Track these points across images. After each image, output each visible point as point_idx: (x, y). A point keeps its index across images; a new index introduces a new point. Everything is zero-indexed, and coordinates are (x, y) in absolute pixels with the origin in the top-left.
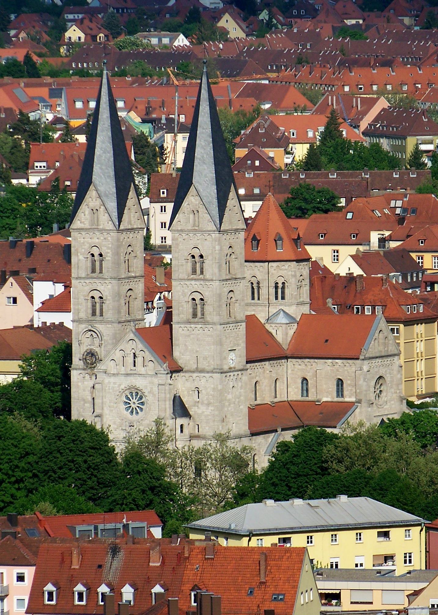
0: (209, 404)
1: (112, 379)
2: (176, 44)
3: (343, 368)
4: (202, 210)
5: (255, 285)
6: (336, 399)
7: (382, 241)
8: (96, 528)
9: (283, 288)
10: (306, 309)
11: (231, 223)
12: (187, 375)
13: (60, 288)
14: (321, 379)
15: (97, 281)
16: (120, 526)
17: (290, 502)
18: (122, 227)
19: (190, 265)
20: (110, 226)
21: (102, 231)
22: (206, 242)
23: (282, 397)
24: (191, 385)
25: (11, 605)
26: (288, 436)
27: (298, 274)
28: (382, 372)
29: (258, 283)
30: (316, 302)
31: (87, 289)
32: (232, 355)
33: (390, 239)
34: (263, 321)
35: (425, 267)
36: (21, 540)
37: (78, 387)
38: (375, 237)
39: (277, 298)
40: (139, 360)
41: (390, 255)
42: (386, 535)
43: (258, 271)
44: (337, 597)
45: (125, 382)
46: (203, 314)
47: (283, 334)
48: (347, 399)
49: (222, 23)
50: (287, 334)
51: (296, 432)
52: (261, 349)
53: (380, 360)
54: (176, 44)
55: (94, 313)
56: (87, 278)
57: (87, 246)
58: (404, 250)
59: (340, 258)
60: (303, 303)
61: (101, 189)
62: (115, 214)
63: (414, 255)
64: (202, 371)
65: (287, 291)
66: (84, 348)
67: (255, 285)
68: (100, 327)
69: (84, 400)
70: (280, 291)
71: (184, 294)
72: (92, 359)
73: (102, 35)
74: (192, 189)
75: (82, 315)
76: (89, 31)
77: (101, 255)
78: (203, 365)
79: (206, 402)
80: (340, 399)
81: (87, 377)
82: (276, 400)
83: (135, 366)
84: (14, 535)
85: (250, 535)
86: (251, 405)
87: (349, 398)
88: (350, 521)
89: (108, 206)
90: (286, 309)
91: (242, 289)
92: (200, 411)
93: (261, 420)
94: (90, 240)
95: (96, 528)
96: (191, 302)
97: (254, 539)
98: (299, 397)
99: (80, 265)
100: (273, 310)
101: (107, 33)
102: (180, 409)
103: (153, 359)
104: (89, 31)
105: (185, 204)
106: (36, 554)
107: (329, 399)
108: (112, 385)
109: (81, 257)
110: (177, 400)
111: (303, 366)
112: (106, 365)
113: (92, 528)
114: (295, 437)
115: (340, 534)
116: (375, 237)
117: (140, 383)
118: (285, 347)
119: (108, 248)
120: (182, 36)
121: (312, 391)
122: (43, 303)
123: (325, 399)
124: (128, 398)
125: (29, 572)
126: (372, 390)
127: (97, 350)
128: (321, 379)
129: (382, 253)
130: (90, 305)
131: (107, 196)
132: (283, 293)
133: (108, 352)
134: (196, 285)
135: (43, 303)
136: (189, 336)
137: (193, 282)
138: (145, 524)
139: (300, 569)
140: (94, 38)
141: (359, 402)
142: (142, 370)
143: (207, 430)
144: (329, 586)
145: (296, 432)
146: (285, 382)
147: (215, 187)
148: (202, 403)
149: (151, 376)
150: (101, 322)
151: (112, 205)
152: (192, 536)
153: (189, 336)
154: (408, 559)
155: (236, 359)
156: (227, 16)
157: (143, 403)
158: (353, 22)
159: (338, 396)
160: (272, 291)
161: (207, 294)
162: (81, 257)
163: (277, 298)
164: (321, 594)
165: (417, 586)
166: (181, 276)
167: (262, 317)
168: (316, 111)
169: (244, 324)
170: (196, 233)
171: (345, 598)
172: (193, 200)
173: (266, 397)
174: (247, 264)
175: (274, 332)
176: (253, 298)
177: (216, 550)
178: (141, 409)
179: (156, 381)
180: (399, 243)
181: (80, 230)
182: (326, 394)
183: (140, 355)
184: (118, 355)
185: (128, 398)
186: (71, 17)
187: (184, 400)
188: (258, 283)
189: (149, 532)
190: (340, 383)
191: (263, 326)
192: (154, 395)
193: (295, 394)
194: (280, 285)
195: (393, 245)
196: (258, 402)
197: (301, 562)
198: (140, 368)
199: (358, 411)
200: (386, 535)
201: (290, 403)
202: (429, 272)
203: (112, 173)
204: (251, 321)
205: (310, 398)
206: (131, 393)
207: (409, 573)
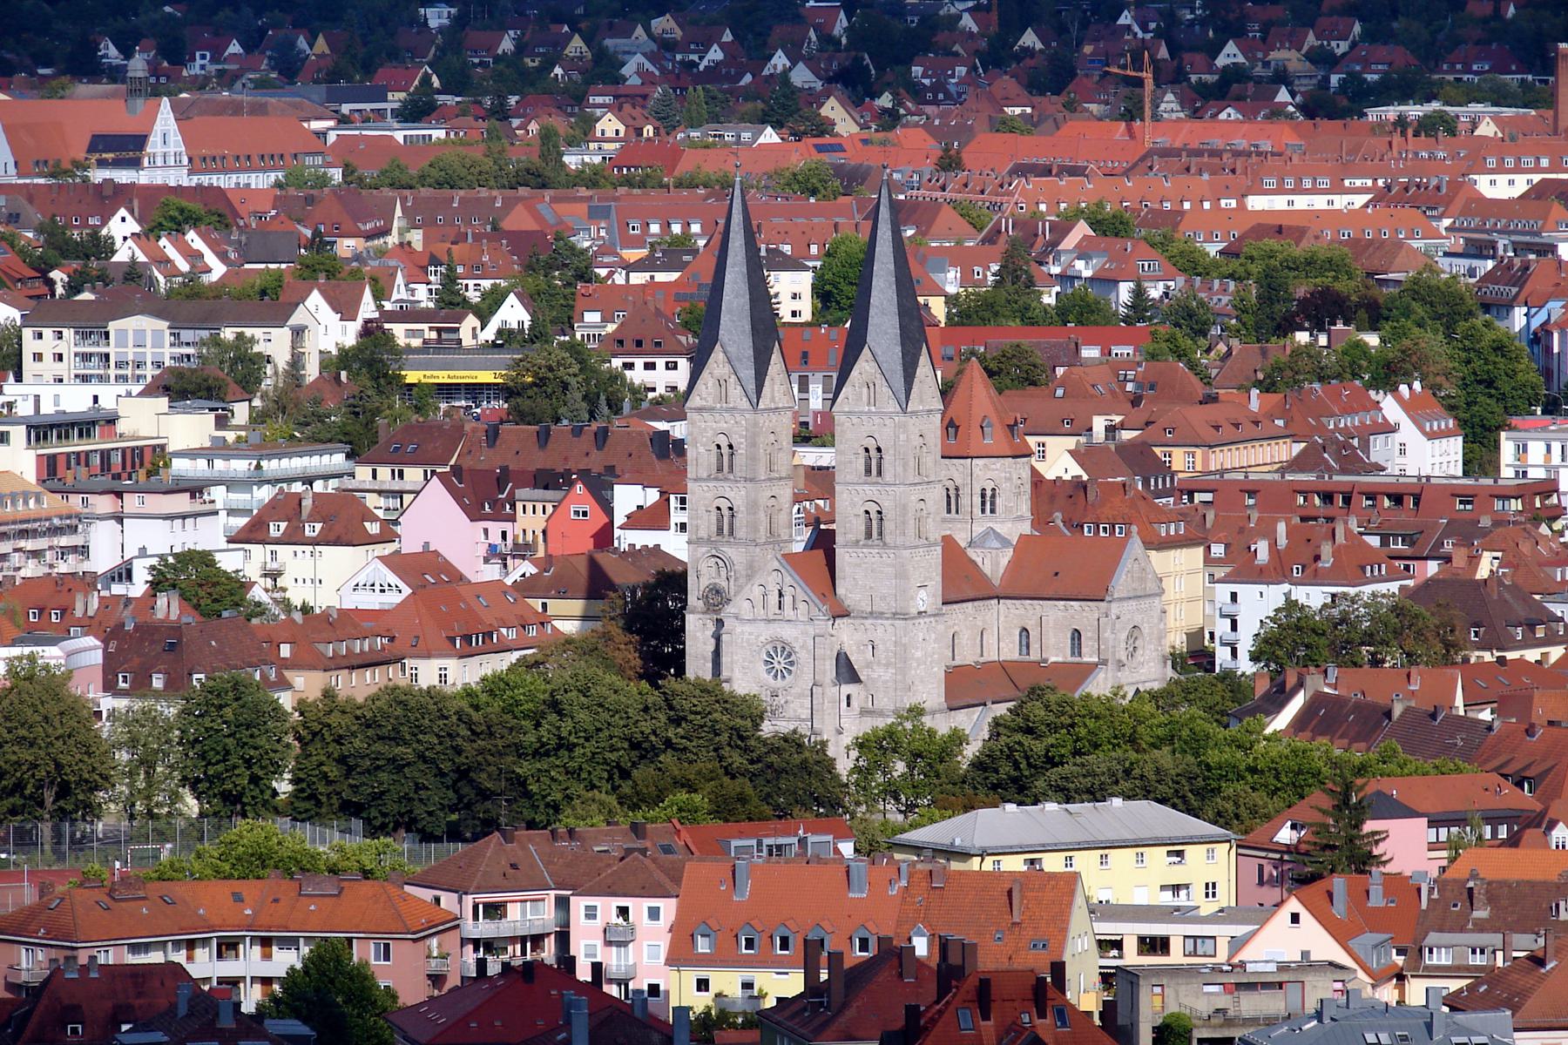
0: (887, 665)
1: (748, 628)
2: (762, 140)
3: (1081, 614)
4: (880, 381)
5: (952, 493)
6: (1070, 659)
7: (1111, 430)
8: (760, 844)
9: (993, 496)
10: (1026, 528)
11: (921, 401)
12: (857, 622)
13: (653, 495)
14: (1052, 630)
16: (795, 840)
17: (1040, 806)
18: (761, 406)
19: (862, 461)
20: (745, 404)
23: (991, 655)
24: (861, 636)
25: (639, 952)
26: (1001, 710)
27: (1015, 477)
28: (1137, 620)
29: (957, 489)
30: (1040, 519)
31: (710, 495)
32: (922, 594)
33: (1122, 426)
34: (963, 544)
35: (1174, 468)
36: (654, 860)
37: (696, 638)
38: (1099, 424)
39: (983, 511)
40: (787, 600)
41: (1123, 448)
42: (1180, 854)
43: (957, 469)
44: (1118, 945)
45: (765, 632)
46: (880, 534)
47: (994, 563)
48: (1086, 659)
49: (825, 111)
50: (998, 564)
51: (1011, 705)
52: (963, 583)
53: (1133, 603)
54: (762, 140)
55: (720, 531)
56: (709, 478)
57: (710, 434)
58: (1144, 443)
59: (1047, 454)
60: (1020, 518)
61: (731, 349)
62: (751, 387)
63: (1157, 450)
64: (881, 615)
65: (998, 501)
66: (704, 582)
67: (952, 493)
68: (729, 552)
70: (988, 501)
71: (853, 505)
72: (717, 599)
73: (650, 128)
74: (866, 350)
75: (703, 533)
76: (631, 122)
77: (731, 447)
78: (880, 606)
80: (1077, 659)
82: (982, 660)
84: (643, 851)
85: (983, 855)
87: (1089, 657)
88: (1128, 835)
89: (741, 375)
90: (998, 528)
91: (936, 495)
92: (875, 675)
93: (964, 685)
95: (760, 844)
96: (863, 515)
97: (989, 860)
98: (1015, 656)
100: (978, 529)
101: (658, 124)
102: (847, 671)
104: (631, 122)
105: (855, 373)
106: (677, 880)
107: (1060, 659)
108: (746, 636)
109: (702, 450)
110: (842, 661)
111: (1022, 611)
112: (739, 606)
113: (754, 842)
114: (1009, 710)
115: (1113, 854)
116: (1099, 424)
117: (788, 633)
118: (997, 582)
120: (769, 129)
121: (1035, 646)
122: (628, 517)
123: (1053, 659)
124: (770, 655)
125: (668, 907)
126: (1123, 645)
127: (724, 584)
128: (1052, 630)
129: (1113, 447)
130: (714, 519)
131: (740, 360)
132: (993, 504)
133: (740, 589)
134: (870, 491)
135: (628, 517)
136: (859, 565)
137: (866, 487)
138: (830, 838)
139: (1070, 904)
140: (639, 132)
141: (1105, 662)
143: (885, 702)
144: (1108, 929)
145: (1011, 705)
146: (994, 632)
147: (898, 349)
148: (879, 663)
151: (748, 373)
152: (897, 856)
153: (859, 565)
154: (1211, 889)
155: (926, 599)
156: (832, 101)
157: (792, 663)
158: (1018, 110)
159: (1073, 654)
160: (977, 500)
161: (887, 505)
162: (702, 450)
163: (983, 511)
164: (1100, 942)
165: (1240, 930)
166: (849, 478)
167: (962, 539)
168: (983, 241)
169: (939, 549)
170: (887, 415)
171: (1176, 946)
173: (967, 655)
174: (947, 461)
175: (979, 561)
176: (949, 511)
177: (948, 876)
178: (790, 672)
180: (1136, 433)
181: (700, 410)
182: (1057, 652)
183: (788, 592)
184: (757, 592)
185: (770, 655)
186: (599, 100)
187: (852, 659)
188: (957, 489)
189: (837, 851)
190: (1076, 635)
191: (963, 552)
193: (1010, 652)
194: (989, 493)
195: (1126, 435)
196: (957, 662)
197: (1072, 893)
198: (788, 611)
199: (1102, 675)
200: (1180, 854)
201: (1003, 666)
202: (1181, 475)
203: (748, 327)
204: (948, 543)
205: (1032, 658)
207: (1221, 911)
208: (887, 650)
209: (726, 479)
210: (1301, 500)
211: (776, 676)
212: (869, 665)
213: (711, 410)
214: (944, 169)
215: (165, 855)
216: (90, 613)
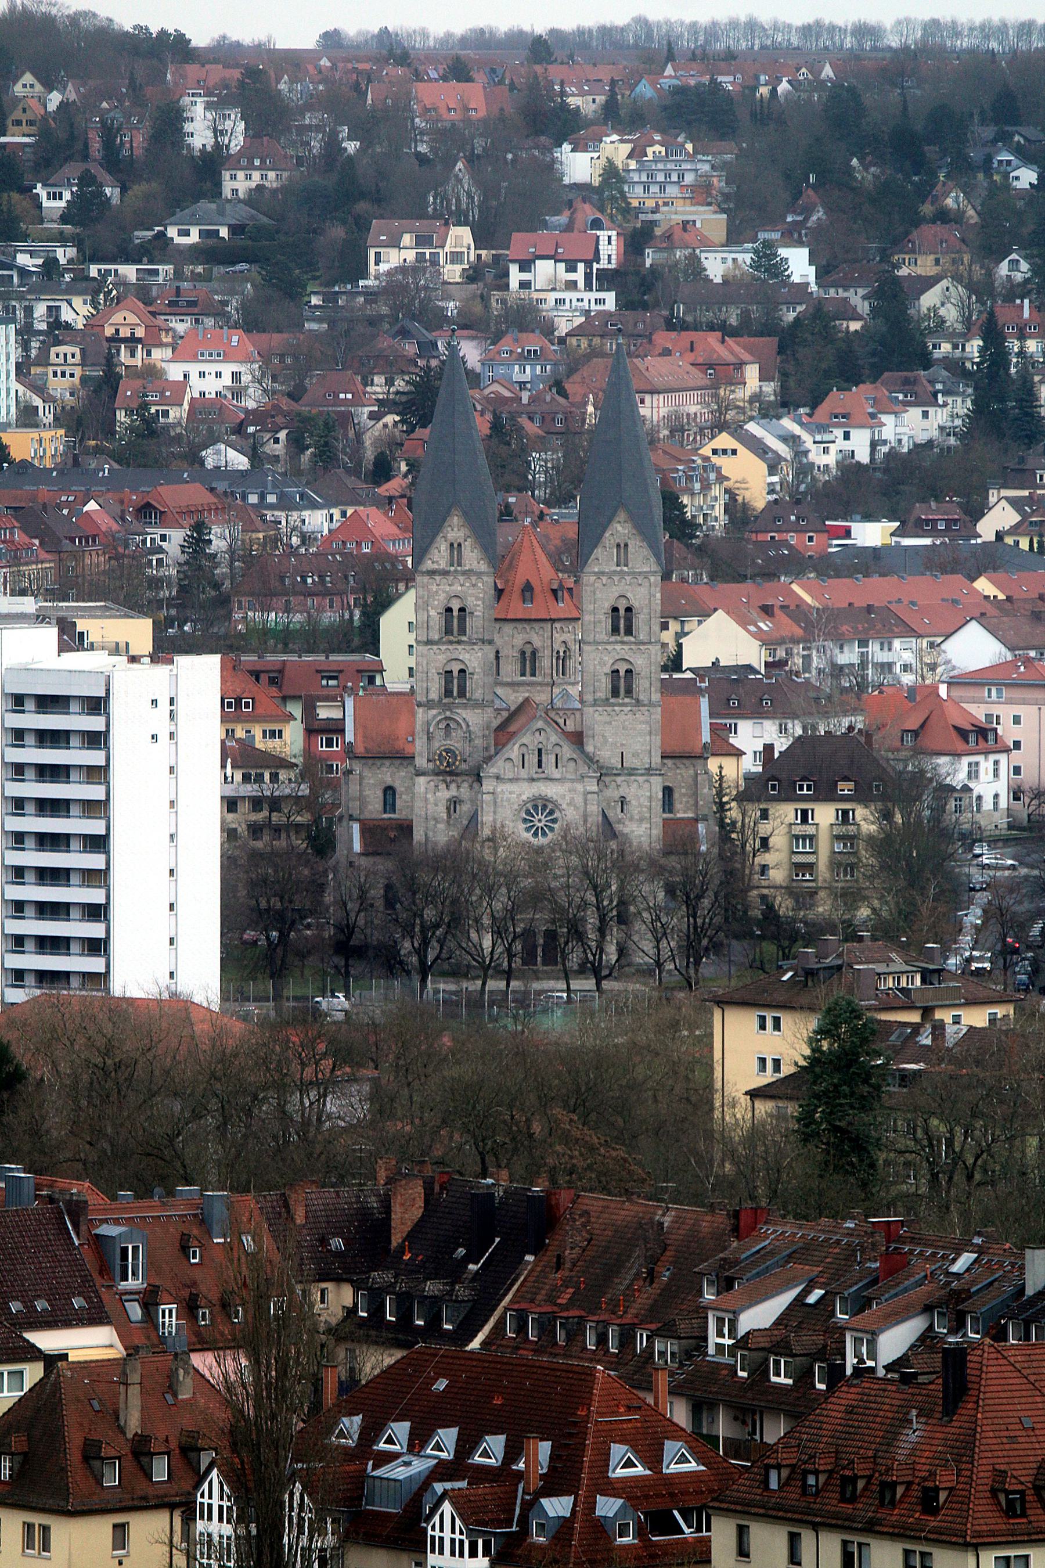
0: (641, 820)
15: (459, 647)
21: (468, 573)
22: (639, 589)
31: (442, 658)
40: (549, 760)
45: (528, 791)
57: (442, 596)
69: (435, 819)
71: (603, 664)
79: (637, 817)
81: (442, 786)
83: (540, 766)
86: (503, 826)
94: (448, 588)
99: (431, 623)
103: (575, 756)
117: (551, 790)
119: (477, 599)
137: (618, 647)
142: (556, 774)
148: (631, 819)
149: (572, 781)
150: (465, 706)
153: (610, 723)
172: (620, 528)
179: (579, 787)
181: (432, 573)
192: (576, 808)
206: (535, 807)
208: (640, 806)
209: (459, 642)
210: (40, 1305)
211: (535, 834)
212: (619, 821)
213: (445, 573)
214: (551, 54)
215: (614, 847)
216: (741, 789)
